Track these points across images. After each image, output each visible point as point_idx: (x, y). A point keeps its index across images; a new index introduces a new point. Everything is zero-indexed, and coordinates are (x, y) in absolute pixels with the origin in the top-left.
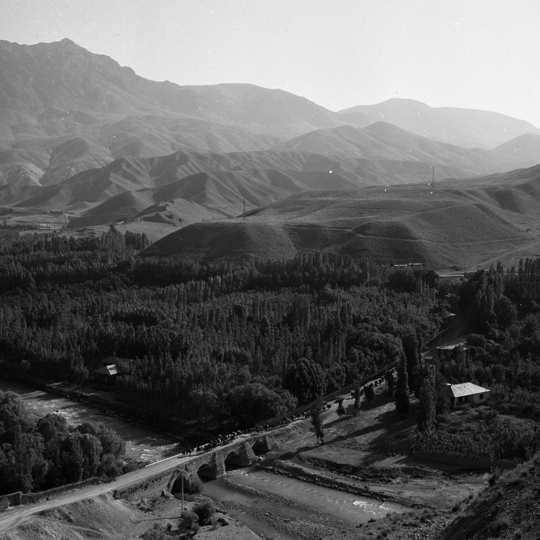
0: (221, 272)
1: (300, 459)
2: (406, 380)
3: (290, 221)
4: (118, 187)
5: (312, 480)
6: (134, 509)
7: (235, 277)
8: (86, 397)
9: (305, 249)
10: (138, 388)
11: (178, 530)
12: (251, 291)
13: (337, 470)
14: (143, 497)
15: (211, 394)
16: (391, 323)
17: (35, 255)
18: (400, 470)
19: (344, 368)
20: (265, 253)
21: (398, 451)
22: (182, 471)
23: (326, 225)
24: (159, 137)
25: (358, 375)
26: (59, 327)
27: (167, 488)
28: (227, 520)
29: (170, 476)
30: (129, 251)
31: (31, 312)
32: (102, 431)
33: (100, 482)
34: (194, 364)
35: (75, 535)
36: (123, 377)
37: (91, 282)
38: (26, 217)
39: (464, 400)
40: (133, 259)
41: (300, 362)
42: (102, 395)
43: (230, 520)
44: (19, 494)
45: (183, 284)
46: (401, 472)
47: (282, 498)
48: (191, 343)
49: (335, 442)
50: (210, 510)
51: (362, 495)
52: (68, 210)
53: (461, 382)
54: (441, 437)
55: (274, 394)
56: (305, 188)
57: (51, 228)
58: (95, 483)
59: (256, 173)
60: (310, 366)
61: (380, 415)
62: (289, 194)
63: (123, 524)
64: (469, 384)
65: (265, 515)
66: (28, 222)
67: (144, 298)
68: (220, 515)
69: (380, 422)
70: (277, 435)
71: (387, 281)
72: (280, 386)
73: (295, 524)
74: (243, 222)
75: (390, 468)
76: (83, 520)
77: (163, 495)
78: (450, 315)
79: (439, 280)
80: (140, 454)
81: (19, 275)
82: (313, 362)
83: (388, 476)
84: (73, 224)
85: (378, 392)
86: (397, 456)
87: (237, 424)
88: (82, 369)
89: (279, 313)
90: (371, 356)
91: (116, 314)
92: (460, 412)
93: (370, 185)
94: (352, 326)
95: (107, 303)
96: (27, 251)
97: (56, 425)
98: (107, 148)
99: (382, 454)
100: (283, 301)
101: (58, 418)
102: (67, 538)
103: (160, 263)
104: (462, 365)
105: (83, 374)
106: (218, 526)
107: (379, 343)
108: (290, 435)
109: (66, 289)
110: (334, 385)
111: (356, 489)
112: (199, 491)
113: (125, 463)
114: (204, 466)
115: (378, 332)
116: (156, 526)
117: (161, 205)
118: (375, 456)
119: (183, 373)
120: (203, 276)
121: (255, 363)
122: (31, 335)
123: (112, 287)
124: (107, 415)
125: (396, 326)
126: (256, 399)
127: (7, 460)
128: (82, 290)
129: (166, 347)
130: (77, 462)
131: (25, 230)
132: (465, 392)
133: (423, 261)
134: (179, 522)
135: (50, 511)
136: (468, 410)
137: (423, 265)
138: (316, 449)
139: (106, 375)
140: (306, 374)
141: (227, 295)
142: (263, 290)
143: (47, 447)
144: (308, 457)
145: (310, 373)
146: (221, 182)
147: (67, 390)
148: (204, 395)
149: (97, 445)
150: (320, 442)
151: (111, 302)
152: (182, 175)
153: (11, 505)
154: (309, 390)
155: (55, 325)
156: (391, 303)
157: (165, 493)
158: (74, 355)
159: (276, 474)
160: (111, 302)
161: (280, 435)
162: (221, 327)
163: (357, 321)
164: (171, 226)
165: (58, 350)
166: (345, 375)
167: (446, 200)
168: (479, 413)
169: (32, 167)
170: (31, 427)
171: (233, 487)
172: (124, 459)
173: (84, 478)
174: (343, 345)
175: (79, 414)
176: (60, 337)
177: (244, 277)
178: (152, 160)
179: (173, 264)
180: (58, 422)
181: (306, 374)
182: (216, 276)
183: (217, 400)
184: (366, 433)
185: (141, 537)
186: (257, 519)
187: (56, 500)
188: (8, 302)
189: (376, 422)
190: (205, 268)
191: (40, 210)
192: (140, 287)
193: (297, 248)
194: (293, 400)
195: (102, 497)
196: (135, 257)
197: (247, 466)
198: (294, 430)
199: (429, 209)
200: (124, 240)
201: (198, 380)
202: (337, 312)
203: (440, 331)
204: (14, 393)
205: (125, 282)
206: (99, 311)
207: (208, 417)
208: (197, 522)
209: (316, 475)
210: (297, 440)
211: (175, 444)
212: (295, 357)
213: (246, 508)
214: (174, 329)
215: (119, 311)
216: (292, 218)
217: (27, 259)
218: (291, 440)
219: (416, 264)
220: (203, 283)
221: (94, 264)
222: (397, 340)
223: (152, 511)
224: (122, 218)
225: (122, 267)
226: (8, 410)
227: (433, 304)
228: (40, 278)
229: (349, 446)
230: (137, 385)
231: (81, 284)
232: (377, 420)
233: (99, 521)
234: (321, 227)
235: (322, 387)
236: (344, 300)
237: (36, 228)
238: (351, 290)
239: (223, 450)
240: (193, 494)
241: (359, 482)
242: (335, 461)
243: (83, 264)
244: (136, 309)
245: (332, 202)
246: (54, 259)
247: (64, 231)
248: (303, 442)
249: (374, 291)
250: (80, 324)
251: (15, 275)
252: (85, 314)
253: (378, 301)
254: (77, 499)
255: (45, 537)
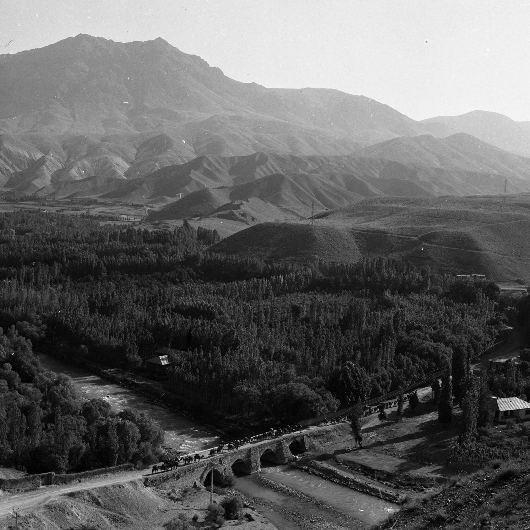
0: (284, 272)
1: (336, 461)
2: (449, 390)
3: (357, 226)
4: (198, 183)
5: (345, 483)
6: (164, 498)
7: (297, 277)
8: (137, 385)
9: (370, 254)
10: (186, 379)
11: (204, 522)
12: (313, 292)
13: (371, 475)
14: (174, 487)
15: (254, 390)
16: (444, 333)
17: (109, 245)
18: (435, 480)
19: (390, 374)
20: (330, 255)
21: (435, 460)
22: (216, 464)
23: (392, 231)
24: (241, 136)
25: (405, 382)
26: (120, 316)
27: (200, 480)
28: (253, 516)
29: (203, 468)
30: (199, 246)
31: (95, 299)
32: (142, 419)
33: (133, 469)
34: (241, 361)
35: (101, 518)
36: (173, 368)
37: (159, 274)
38: (108, 208)
39: (509, 414)
40: (201, 254)
41: (345, 365)
42: (153, 384)
43: (258, 516)
44: (51, 474)
45: (245, 281)
46: (435, 482)
47: (312, 498)
48: (241, 339)
49: (373, 447)
50: (238, 505)
51: (393, 502)
52: (149, 203)
53: (508, 396)
54: (479, 450)
55: (315, 394)
56: (378, 193)
57: (130, 220)
58: (128, 469)
59: (332, 177)
60: (354, 370)
61: (423, 424)
62: (363, 198)
63: (150, 511)
64: (516, 398)
65: (293, 514)
66: (110, 213)
67: (206, 292)
68: (248, 511)
69: (421, 431)
70: (316, 436)
71: (447, 290)
72: (323, 387)
73: (321, 526)
74: (311, 224)
75: (425, 477)
76: (111, 504)
77: (195, 486)
78: (508, 328)
79: (499, 293)
80: (181, 445)
81: (92, 263)
82: (358, 366)
83: (421, 485)
84: (153, 217)
85: (424, 400)
86: (433, 465)
87: (279, 423)
88: (136, 357)
89: (336, 316)
90: (420, 364)
91: (177, 306)
92: (504, 426)
93: (445, 195)
94: (404, 333)
95: (169, 295)
96: (101, 240)
97: (100, 410)
98: (191, 145)
99: (418, 462)
100: (340, 304)
101: (103, 403)
102: (93, 520)
103: (227, 259)
104: (512, 379)
105: (136, 362)
106: (244, 521)
107: (429, 351)
108: (329, 437)
109: (135, 280)
110: (378, 390)
111: (387, 495)
112: (232, 485)
113: (163, 451)
114: (238, 460)
115: (430, 340)
116: (181, 517)
117: (236, 203)
118: (411, 463)
119: (229, 368)
120: (266, 275)
121: (305, 364)
122: (92, 320)
123: (178, 281)
124: (154, 404)
125: (449, 335)
126: (297, 398)
127: (47, 440)
128: (150, 281)
129: (218, 341)
130: (112, 448)
131: (106, 220)
132: (511, 406)
133: (487, 273)
134: (206, 515)
135: (80, 493)
136: (512, 425)
137: (486, 277)
138: (353, 453)
139: (158, 365)
140: (350, 377)
141: (288, 295)
142: (325, 292)
143: (90, 431)
144: (344, 460)
145: (354, 377)
146: (296, 184)
147: (120, 376)
148: (248, 391)
149: (134, 432)
150: (358, 446)
151: (173, 295)
152: (260, 175)
153: (43, 485)
154: (352, 393)
155: (117, 314)
156: (449, 313)
157: (197, 485)
158: (129, 343)
159: (311, 474)
160: (173, 295)
161: (319, 436)
162: (275, 326)
163: (409, 328)
164: (244, 224)
165: (115, 337)
166: (391, 381)
167: (516, 213)
168: (523, 429)
169: (119, 160)
170: (76, 409)
171: (266, 484)
172: (164, 448)
173: (118, 463)
174: (392, 351)
175: (128, 401)
176: (118, 325)
177: (307, 278)
178: (232, 159)
179: (239, 261)
180: (102, 407)
181: (350, 377)
182: (279, 276)
183: (260, 397)
184: (405, 441)
185: (164, 526)
186: (284, 517)
187: (87, 483)
188: (79, 288)
189: (417, 430)
190: (270, 267)
191: (122, 202)
192: (205, 282)
193: (362, 253)
194: (335, 402)
195: (133, 483)
196: (203, 253)
197: (283, 464)
198: (334, 432)
199: (498, 221)
200: (196, 235)
201: (244, 376)
202: (390, 318)
203: (495, 343)
204: (66, 376)
205: (192, 276)
206: (161, 302)
207: (251, 413)
208: (223, 515)
209: (349, 478)
210: (335, 442)
211: (216, 437)
212: (343, 359)
213: (275, 505)
214: (229, 325)
215: (180, 303)
216: (360, 223)
217: (101, 248)
218: (329, 442)
219: (479, 275)
220: (266, 281)
221: (163, 257)
222: (447, 349)
223: (181, 501)
224: (198, 214)
225: (190, 261)
226: (57, 392)
227: (491, 316)
228: (111, 268)
229: (386, 452)
230: (186, 376)
231: (149, 275)
232: (418, 428)
233: (127, 506)
234: (388, 233)
235: (365, 392)
236: (402, 307)
237: (117, 219)
238: (411, 297)
239: (259, 447)
240: (225, 487)
241: (392, 488)
242: (370, 466)
243: (153, 257)
244: (195, 303)
245: (402, 210)
246: (127, 250)
247: (142, 224)
248: (341, 444)
249: (433, 300)
250: (140, 314)
251: (87, 263)
252: (147, 304)
253: (435, 309)
254: (108, 484)
255: (71, 518)
